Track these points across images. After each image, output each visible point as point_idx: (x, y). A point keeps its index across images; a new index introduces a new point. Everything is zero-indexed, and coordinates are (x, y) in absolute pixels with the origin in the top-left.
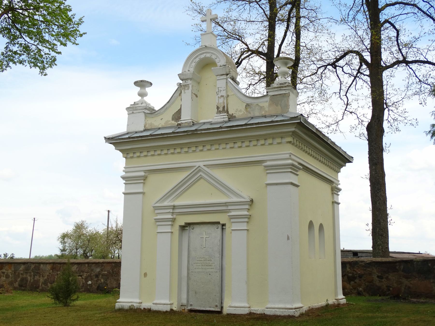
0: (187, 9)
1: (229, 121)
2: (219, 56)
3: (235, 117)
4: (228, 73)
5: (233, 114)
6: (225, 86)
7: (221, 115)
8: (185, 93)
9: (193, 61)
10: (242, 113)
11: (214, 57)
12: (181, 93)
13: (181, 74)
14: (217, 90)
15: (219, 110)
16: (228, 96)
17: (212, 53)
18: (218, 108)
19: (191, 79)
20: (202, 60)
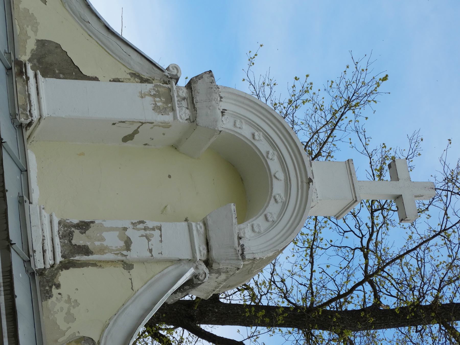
0: (362, 65)
1: (32, 274)
2: (274, 232)
3: (48, 295)
4: (215, 266)
5: (58, 286)
6: (166, 255)
7: (57, 240)
8: (142, 96)
9: (258, 128)
10: (63, 326)
11: (273, 209)
12: (143, 80)
13: (213, 82)
14: (150, 224)
15: (77, 232)
16: (128, 266)
17: (285, 205)
18: (84, 226)
19: (193, 120)
20: (260, 162)
